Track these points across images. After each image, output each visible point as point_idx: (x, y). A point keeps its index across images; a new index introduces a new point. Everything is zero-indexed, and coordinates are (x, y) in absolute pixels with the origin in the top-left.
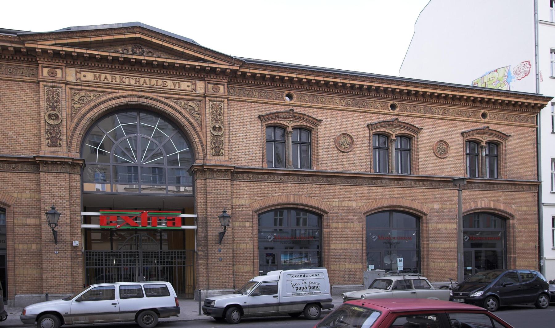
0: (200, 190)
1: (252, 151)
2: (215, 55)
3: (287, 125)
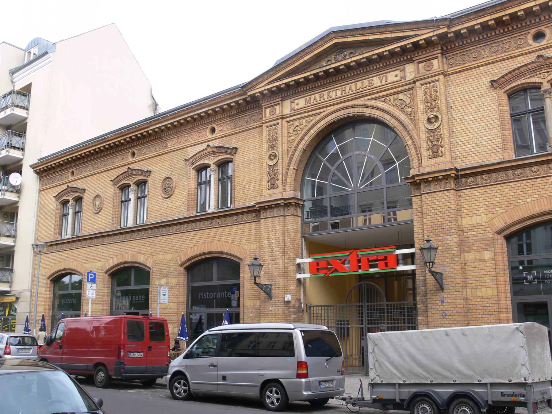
0: (417, 212)
1: (485, 138)
2: (414, 27)
3: (539, 81)
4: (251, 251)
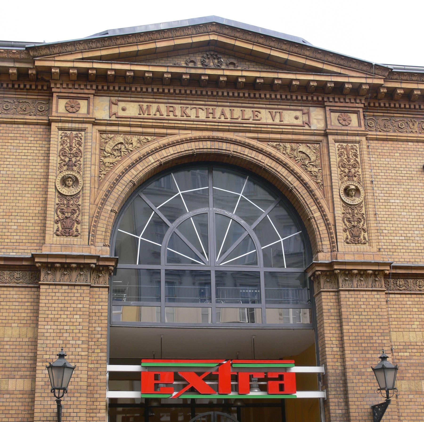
0: (329, 314)
1: (417, 232)
4: (6, 339)
